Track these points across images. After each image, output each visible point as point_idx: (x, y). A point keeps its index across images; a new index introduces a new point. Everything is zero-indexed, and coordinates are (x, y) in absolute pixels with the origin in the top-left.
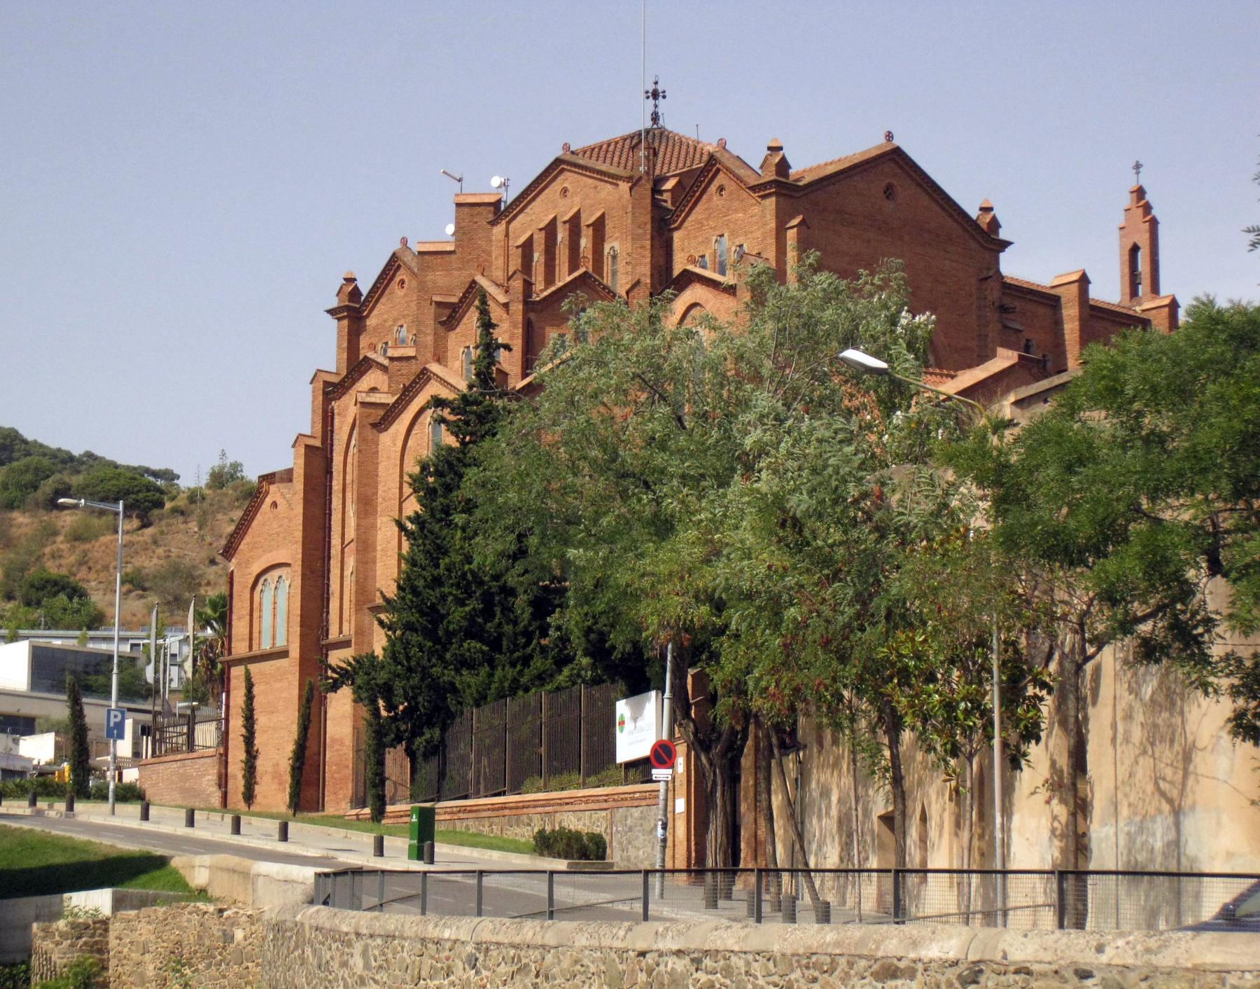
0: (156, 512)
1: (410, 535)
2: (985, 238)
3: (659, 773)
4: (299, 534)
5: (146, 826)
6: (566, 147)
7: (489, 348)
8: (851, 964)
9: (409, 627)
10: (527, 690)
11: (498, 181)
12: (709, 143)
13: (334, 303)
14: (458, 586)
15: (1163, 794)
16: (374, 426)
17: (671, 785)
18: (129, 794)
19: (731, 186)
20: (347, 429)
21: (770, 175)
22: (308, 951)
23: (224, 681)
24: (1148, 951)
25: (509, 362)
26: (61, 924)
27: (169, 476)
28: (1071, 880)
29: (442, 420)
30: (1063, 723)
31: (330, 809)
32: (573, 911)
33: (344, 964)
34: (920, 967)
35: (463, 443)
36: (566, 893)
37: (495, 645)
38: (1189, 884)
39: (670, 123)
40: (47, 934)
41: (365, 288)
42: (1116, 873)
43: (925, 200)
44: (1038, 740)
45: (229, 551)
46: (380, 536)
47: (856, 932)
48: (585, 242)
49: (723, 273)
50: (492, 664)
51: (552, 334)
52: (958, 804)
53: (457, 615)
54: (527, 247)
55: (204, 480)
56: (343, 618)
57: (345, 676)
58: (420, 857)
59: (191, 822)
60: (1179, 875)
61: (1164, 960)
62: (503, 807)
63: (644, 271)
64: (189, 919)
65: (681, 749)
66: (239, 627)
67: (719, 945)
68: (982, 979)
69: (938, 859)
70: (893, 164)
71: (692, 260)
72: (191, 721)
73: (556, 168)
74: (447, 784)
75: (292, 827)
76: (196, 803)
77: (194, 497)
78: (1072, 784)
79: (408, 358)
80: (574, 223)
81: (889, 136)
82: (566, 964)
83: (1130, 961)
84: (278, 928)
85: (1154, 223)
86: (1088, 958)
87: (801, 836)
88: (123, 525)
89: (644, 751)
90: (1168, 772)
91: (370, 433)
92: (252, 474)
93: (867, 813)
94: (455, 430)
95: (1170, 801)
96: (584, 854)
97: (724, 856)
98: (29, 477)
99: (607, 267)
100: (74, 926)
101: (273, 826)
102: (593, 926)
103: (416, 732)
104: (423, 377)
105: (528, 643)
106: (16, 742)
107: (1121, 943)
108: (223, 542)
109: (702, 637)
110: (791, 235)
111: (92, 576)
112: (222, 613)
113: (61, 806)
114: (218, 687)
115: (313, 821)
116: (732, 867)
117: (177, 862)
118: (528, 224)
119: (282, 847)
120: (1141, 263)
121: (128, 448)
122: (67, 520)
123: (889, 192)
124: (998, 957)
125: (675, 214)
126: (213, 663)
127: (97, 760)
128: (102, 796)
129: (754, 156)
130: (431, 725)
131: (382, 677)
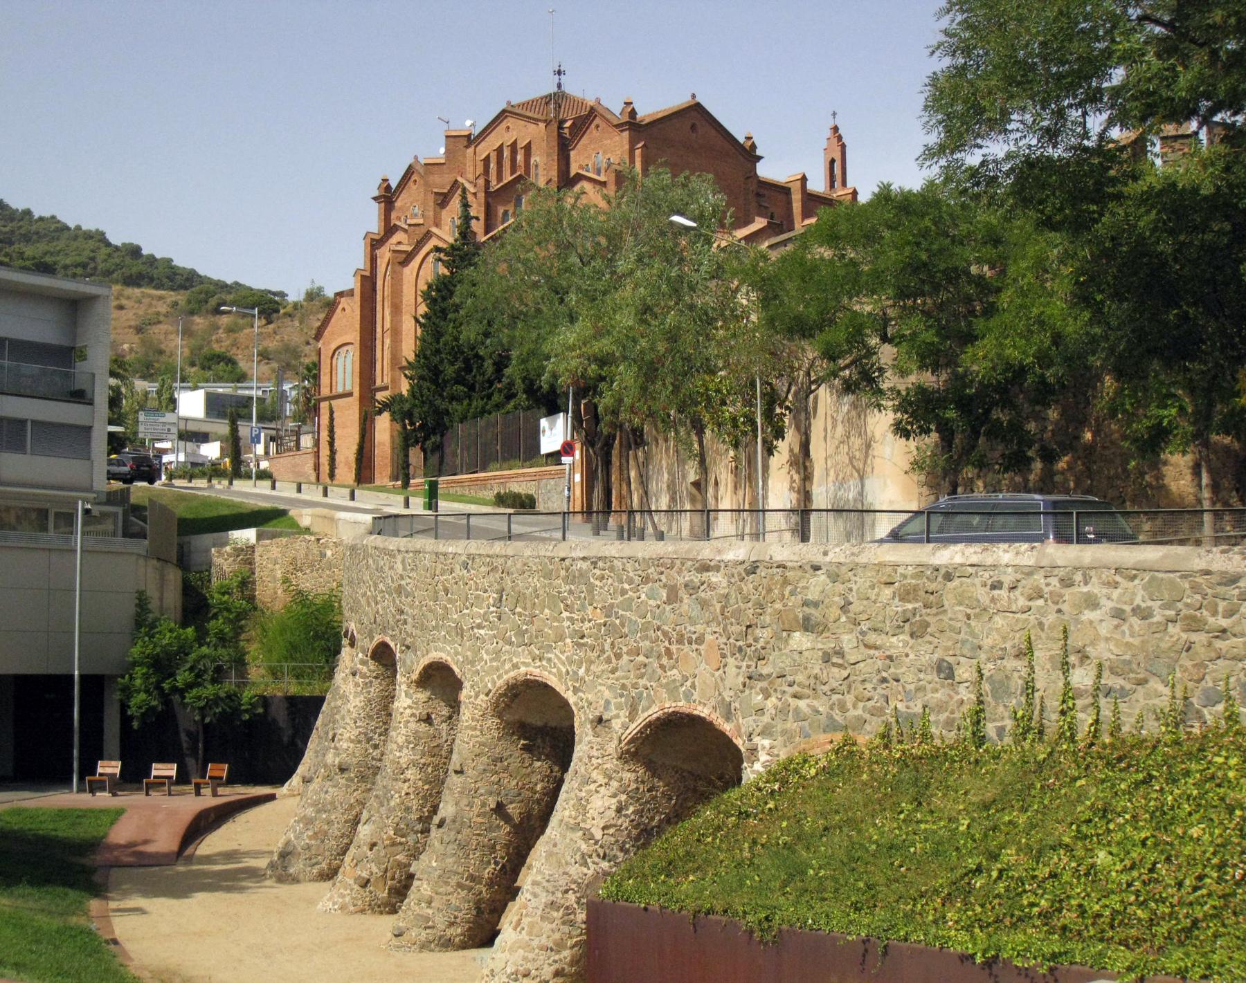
0: (275, 315)
1: (422, 325)
2: (749, 155)
3: (565, 459)
4: (358, 326)
5: (274, 493)
6: (509, 103)
7: (467, 218)
8: (683, 564)
9: (422, 378)
10: (490, 413)
11: (469, 124)
12: (590, 100)
13: (376, 193)
14: (450, 353)
15: (854, 467)
17: (572, 465)
18: (263, 475)
19: (603, 125)
20: (384, 266)
21: (626, 119)
22: (371, 561)
23: (316, 410)
24: (853, 554)
25: (477, 226)
26: (228, 548)
27: (282, 295)
28: (803, 513)
29: (440, 260)
30: (798, 428)
31: (378, 483)
32: (520, 537)
33: (391, 568)
34: (722, 565)
35: (452, 273)
36: (516, 529)
37: (472, 388)
38: (868, 518)
39: (568, 89)
40: (220, 554)
41: (394, 185)
42: (827, 511)
43: (713, 132)
44: (783, 438)
45: (318, 335)
47: (676, 544)
49: (599, 173)
50: (470, 397)
51: (501, 210)
52: (736, 476)
53: (450, 371)
54: (487, 160)
55: (302, 297)
56: (383, 374)
57: (386, 406)
58: (430, 509)
59: (299, 490)
60: (862, 511)
61: (862, 559)
62: (477, 480)
63: (554, 174)
64: (300, 546)
65: (578, 446)
66: (325, 380)
67: (607, 554)
68: (758, 571)
69: (725, 504)
70: (695, 114)
71: (581, 167)
72: (298, 434)
73: (503, 115)
74: (445, 467)
75: (357, 492)
76: (301, 480)
77: (296, 306)
78: (802, 460)
79: (418, 225)
80: (514, 146)
81: (694, 96)
82: (519, 566)
83: (842, 560)
84: (353, 548)
85: (843, 146)
86: (818, 559)
87: (646, 493)
88: (257, 323)
89: (557, 447)
90: (857, 454)
91: (398, 268)
92: (330, 293)
93: (684, 477)
94: (447, 265)
95: (858, 471)
96: (523, 506)
97: (602, 504)
98: (203, 296)
99: (533, 170)
100: (235, 549)
101: (347, 492)
102: (534, 544)
103: (426, 438)
104: (428, 235)
105: (490, 387)
106: (198, 447)
107: (837, 550)
108: (314, 332)
109: (591, 382)
110: (638, 152)
111: (239, 352)
112: (313, 373)
113: (225, 482)
114: (312, 414)
115: (369, 489)
116: (607, 510)
117: (293, 513)
118: (487, 148)
119: (352, 504)
120: (836, 169)
121: (258, 280)
122: (225, 320)
123: (693, 127)
124: (767, 559)
125: (571, 141)
126: (309, 400)
127: (244, 457)
128: (248, 476)
129: (616, 107)
130: (435, 434)
131: (407, 407)
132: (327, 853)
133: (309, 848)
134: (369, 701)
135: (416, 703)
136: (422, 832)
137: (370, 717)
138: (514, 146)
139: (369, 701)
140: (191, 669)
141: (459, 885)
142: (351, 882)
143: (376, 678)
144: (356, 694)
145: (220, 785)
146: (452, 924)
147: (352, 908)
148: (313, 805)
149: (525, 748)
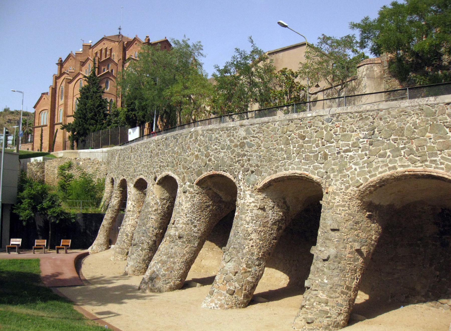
1: (79, 101)
6: (105, 36)
9: (80, 118)
11: (90, 42)
13: (57, 62)
19: (138, 43)
37: (97, 121)
39: (123, 33)
41: (63, 60)
46: (69, 103)
48: (108, 53)
50: (96, 124)
51: (103, 68)
53: (89, 115)
54: (96, 53)
66: (37, 121)
80: (106, 49)
81: (166, 38)
91: (67, 84)
131: (73, 127)
132: (173, 278)
133: (164, 275)
134: (193, 205)
135: (257, 200)
136: (258, 266)
137: (193, 212)
138: (106, 49)
139: (193, 205)
140: (49, 201)
141: (342, 292)
142: (225, 292)
143: (197, 194)
144: (186, 202)
145: (68, 249)
146: (339, 314)
147: (226, 306)
148: (165, 255)
149: (369, 217)
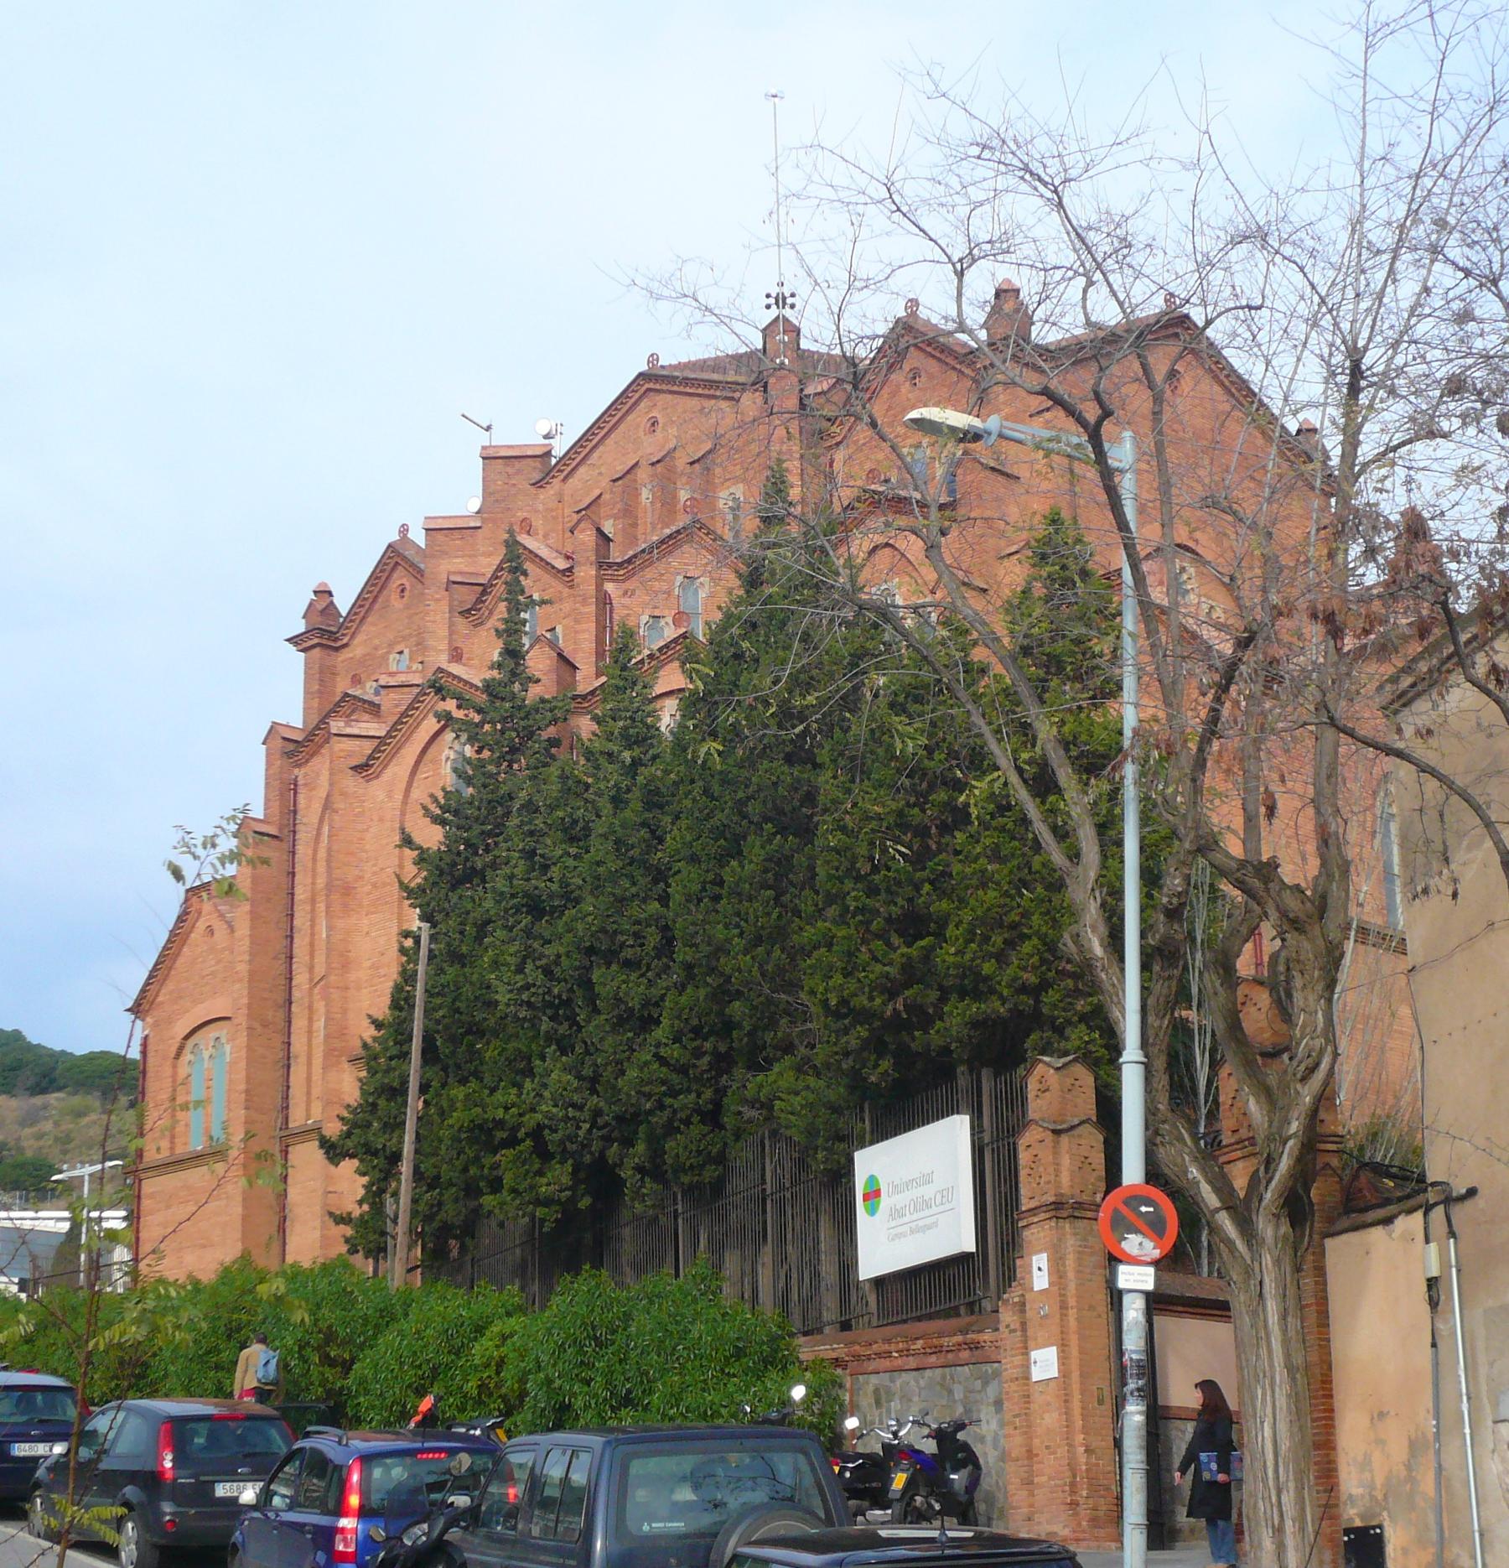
6: (653, 359)
16: (360, 769)
118: (588, 482)
